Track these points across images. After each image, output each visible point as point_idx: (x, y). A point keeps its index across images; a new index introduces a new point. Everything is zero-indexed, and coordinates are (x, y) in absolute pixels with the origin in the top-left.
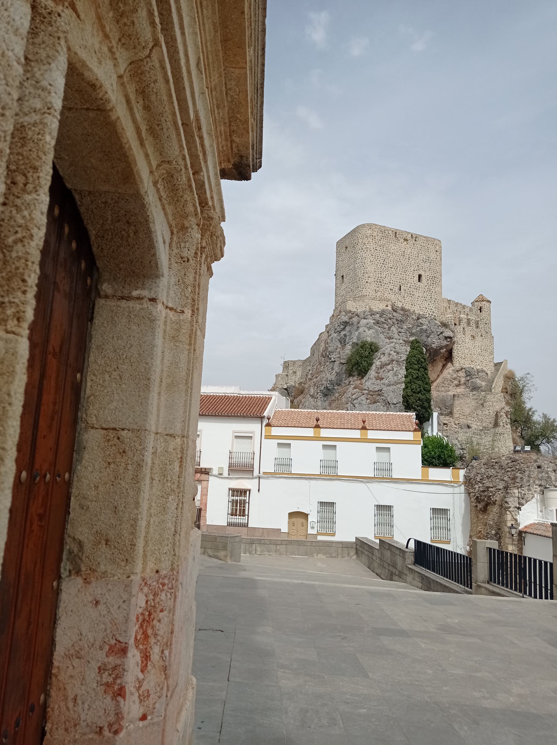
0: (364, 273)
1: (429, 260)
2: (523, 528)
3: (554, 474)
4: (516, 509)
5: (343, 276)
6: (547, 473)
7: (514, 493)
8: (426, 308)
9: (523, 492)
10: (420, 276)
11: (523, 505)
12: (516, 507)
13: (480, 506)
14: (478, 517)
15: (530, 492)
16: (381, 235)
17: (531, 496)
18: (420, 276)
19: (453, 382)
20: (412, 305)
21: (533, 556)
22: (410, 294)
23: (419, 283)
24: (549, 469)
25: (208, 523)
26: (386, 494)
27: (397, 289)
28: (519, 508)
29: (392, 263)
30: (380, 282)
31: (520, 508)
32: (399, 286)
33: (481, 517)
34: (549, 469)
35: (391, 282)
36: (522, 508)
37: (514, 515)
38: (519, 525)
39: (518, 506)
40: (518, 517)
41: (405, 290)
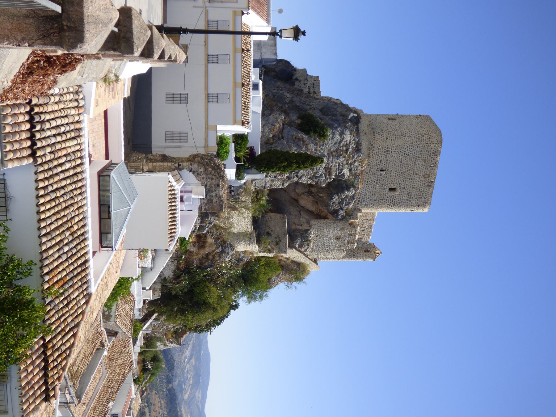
0: (395, 135)
3: (214, 195)
8: (365, 195)
10: (391, 190)
11: (193, 174)
18: (391, 190)
21: (216, 19)
23: (388, 189)
27: (380, 167)
28: (191, 171)
32: (384, 169)
36: (191, 173)
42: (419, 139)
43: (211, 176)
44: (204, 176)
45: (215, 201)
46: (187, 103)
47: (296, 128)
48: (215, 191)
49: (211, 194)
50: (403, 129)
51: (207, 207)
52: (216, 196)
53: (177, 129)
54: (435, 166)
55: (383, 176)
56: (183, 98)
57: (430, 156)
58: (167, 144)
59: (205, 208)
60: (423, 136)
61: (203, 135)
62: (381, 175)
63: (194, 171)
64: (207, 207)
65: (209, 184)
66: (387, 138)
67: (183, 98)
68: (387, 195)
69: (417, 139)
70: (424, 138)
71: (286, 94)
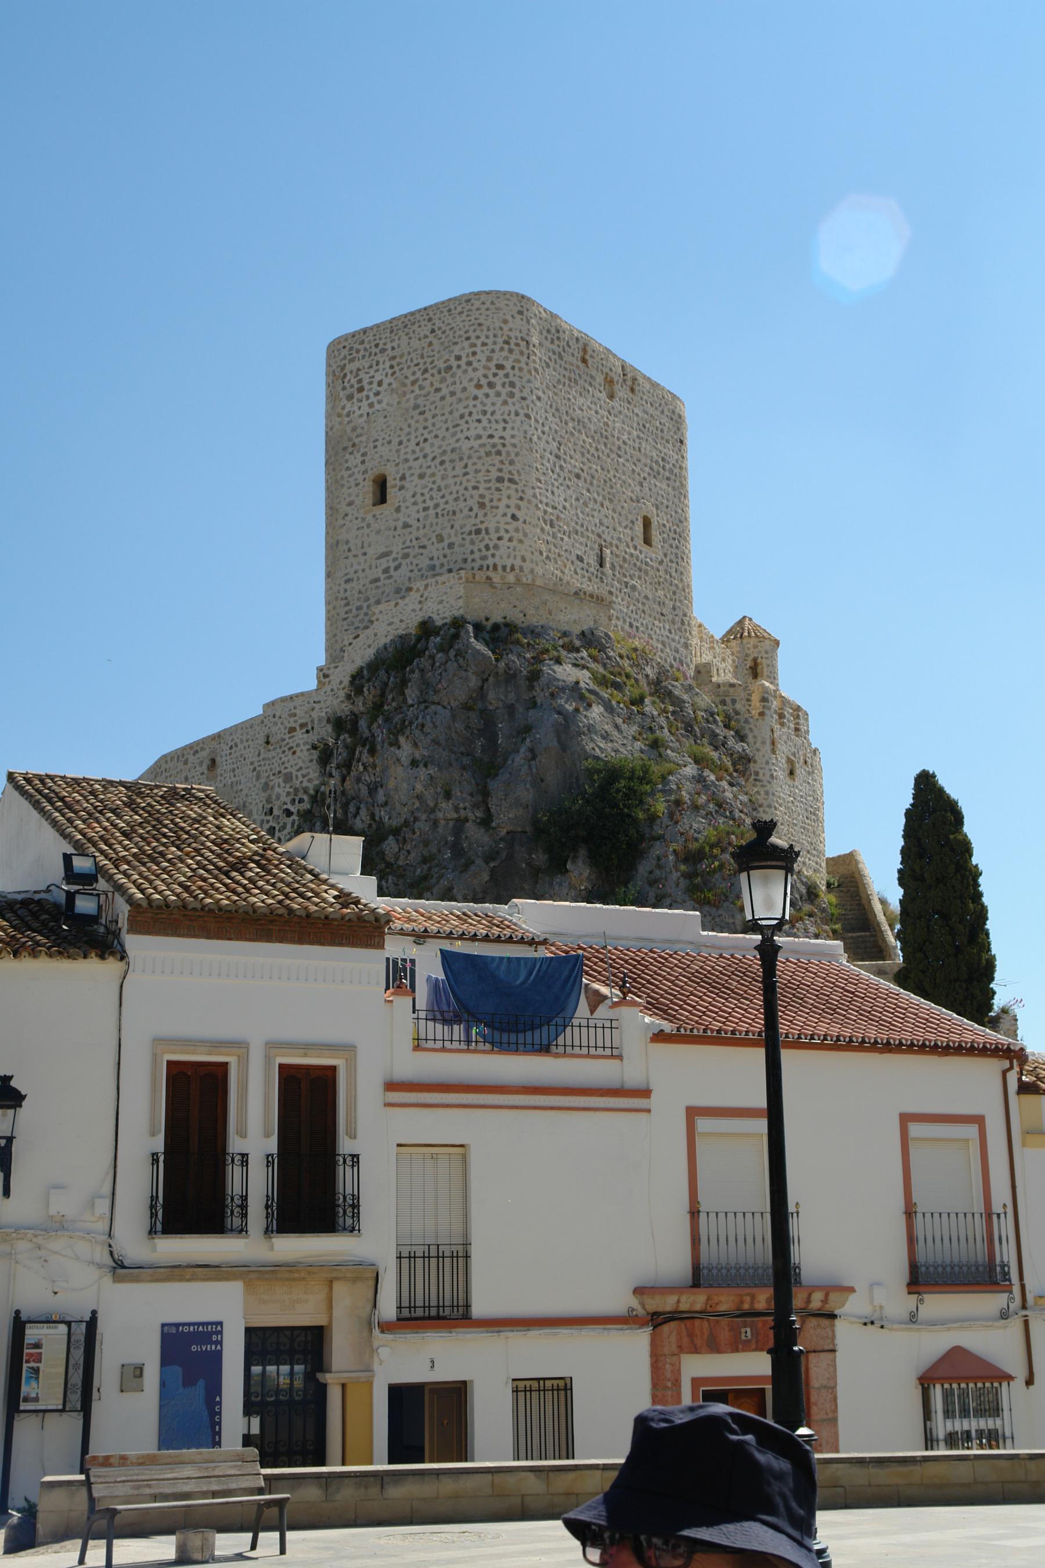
0: (500, 480)
23: (645, 548)
27: (592, 560)
29: (578, 456)
42: (512, 384)
50: (465, 445)
54: (585, 345)
60: (500, 367)
62: (613, 567)
66: (514, 517)
69: (512, 395)
70: (508, 365)
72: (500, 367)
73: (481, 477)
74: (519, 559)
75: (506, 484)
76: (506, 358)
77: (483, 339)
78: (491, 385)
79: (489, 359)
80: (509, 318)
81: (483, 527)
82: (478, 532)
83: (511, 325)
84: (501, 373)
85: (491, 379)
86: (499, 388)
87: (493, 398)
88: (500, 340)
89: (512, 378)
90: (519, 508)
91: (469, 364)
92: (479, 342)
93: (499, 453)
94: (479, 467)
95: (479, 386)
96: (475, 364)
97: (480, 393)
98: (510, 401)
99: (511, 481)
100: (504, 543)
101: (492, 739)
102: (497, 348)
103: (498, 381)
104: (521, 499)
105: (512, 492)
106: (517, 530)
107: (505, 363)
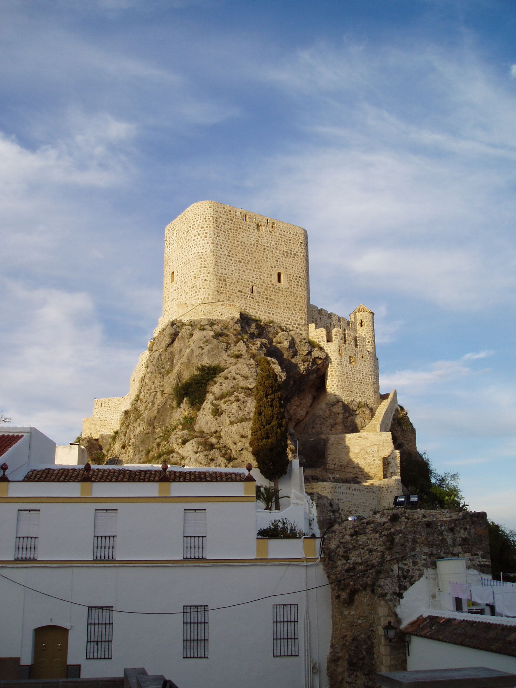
0: (201, 267)
1: (291, 254)
2: (406, 628)
3: (450, 535)
4: (395, 597)
5: (173, 273)
6: (441, 533)
7: (392, 571)
9: (406, 568)
10: (279, 275)
11: (405, 589)
12: (395, 593)
13: (344, 595)
14: (342, 614)
15: (416, 567)
16: (225, 216)
17: (417, 573)
18: (279, 275)
19: (327, 421)
20: (269, 313)
21: (12, 543)
22: (267, 299)
23: (278, 284)
24: (443, 528)
25: (464, 561)
26: (194, 585)
28: (400, 595)
30: (225, 280)
31: (401, 594)
32: (250, 287)
33: (346, 613)
34: (443, 528)
35: (240, 280)
36: (405, 594)
37: (392, 606)
38: (399, 621)
39: (397, 590)
40: (398, 610)
41: (259, 293)
43: (409, 545)
44: (409, 561)
45: (463, 534)
46: (205, 608)
47: (199, 410)
48: (441, 533)
49: (450, 541)
51: (480, 553)
52: (452, 530)
53: (266, 631)
55: (260, 290)
56: (195, 617)
57: (231, 220)
58: (302, 653)
59: (483, 557)
60: (202, 228)
61: (291, 571)
63: (400, 587)
64: (480, 553)
65: (426, 550)
67: (195, 617)
68: (287, 285)
70: (205, 226)
71: (137, 432)
72: (202, 228)
73: (195, 267)
74: (207, 295)
75: (203, 268)
76: (204, 224)
77: (197, 219)
78: (199, 234)
79: (199, 225)
80: (206, 210)
81: (195, 285)
82: (193, 287)
83: (206, 212)
84: (202, 229)
85: (199, 232)
86: (201, 235)
87: (199, 239)
88: (202, 219)
89: (206, 231)
90: (208, 276)
91: (193, 228)
92: (195, 220)
93: (201, 258)
94: (194, 264)
95: (195, 236)
96: (194, 228)
97: (195, 238)
98: (205, 239)
99: (205, 267)
100: (202, 289)
101: (172, 362)
102: (201, 221)
103: (201, 233)
104: (209, 273)
105: (205, 271)
106: (207, 285)
107: (204, 226)
